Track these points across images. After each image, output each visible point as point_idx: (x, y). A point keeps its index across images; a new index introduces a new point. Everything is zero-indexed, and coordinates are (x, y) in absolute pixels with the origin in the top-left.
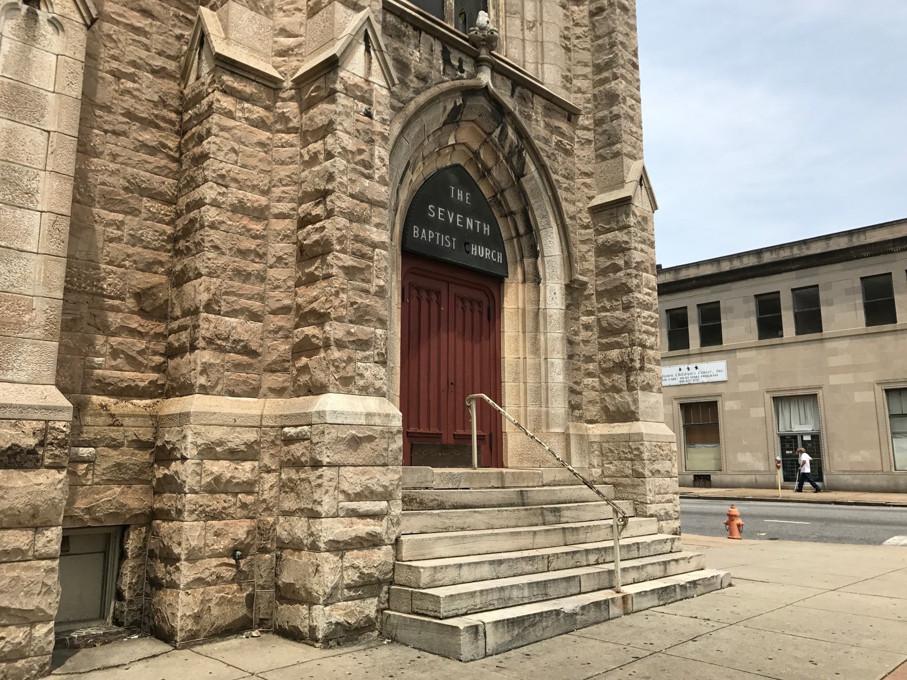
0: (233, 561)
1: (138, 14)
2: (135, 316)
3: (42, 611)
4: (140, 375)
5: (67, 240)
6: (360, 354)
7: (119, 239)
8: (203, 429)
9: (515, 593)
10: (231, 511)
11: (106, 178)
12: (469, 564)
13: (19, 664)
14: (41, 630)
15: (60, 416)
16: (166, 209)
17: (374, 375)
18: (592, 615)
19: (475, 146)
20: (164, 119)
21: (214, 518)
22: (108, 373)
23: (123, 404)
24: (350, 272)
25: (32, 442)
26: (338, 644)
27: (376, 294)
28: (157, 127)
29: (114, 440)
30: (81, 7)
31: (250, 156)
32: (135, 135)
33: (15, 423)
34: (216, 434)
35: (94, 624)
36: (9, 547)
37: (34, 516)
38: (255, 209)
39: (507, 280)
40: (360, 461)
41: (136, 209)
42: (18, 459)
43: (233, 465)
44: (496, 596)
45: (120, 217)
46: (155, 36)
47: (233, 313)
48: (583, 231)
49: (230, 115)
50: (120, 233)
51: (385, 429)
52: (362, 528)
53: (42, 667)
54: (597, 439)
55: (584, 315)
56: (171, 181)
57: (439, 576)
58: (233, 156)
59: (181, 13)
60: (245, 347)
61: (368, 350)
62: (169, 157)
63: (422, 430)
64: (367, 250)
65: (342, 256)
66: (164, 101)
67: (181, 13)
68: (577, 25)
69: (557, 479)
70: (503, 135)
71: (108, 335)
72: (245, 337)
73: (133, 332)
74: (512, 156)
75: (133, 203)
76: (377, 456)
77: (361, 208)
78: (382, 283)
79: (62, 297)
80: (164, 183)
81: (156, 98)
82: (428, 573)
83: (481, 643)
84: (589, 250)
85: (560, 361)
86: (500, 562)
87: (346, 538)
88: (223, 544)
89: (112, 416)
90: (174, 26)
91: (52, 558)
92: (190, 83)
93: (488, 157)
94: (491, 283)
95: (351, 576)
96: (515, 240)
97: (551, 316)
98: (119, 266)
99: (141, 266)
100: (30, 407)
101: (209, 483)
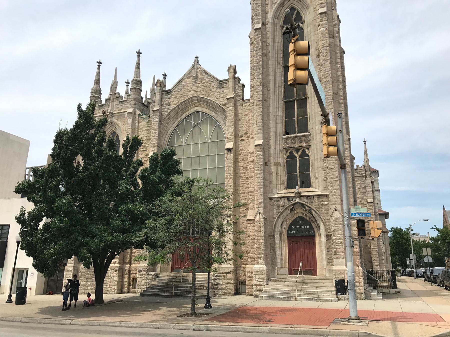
18: (287, 299)
24: (258, 248)
34: (249, 270)
52: (259, 283)
70: (305, 208)
77: (258, 238)
88: (251, 284)
94: (313, 237)
95: (257, 289)
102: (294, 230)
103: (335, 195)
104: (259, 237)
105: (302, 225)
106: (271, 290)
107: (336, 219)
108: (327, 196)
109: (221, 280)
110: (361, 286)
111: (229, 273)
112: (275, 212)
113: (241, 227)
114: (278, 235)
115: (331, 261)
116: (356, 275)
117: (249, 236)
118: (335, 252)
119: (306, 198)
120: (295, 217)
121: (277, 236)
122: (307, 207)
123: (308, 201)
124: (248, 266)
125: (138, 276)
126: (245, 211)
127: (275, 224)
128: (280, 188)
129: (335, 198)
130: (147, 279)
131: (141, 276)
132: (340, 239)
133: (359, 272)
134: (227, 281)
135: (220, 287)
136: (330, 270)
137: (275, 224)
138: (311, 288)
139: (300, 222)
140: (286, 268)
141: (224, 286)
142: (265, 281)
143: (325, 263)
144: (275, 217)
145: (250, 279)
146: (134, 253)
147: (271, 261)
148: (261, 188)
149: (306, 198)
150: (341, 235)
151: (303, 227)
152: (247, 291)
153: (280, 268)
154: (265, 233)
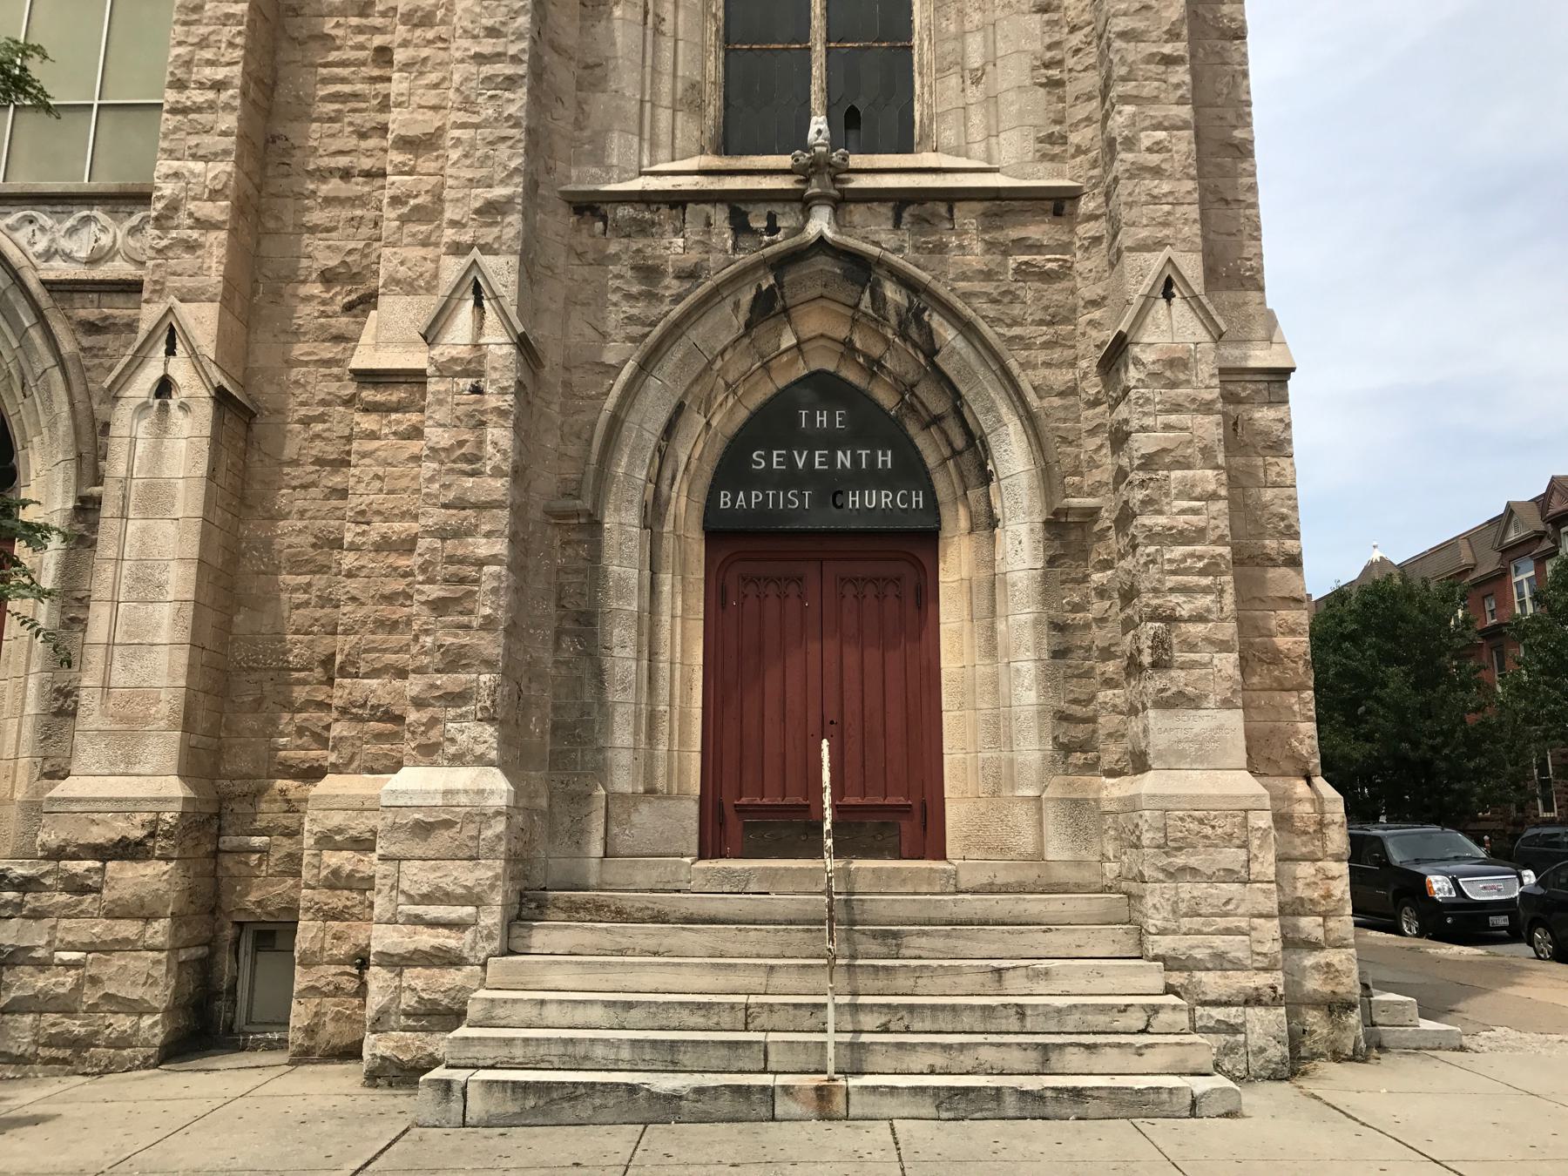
0: (356, 972)
6: (452, 712)
7: (307, 604)
8: (321, 814)
9: (599, 1051)
10: (356, 910)
11: (294, 540)
12: (561, 1002)
14: (147, 1021)
15: (170, 806)
17: (475, 738)
18: (725, 1105)
19: (842, 332)
21: (335, 917)
22: (292, 754)
24: (439, 606)
25: (139, 834)
26: (390, 1085)
27: (481, 628)
31: (400, 477)
33: (128, 814)
34: (337, 819)
37: (142, 907)
38: (404, 541)
39: (942, 534)
40: (431, 853)
43: (358, 856)
44: (556, 1050)
45: (305, 579)
47: (374, 673)
48: (1090, 413)
49: (372, 435)
51: (474, 811)
52: (427, 939)
53: (147, 1058)
54: (1114, 807)
55: (1098, 571)
57: (499, 1012)
58: (377, 484)
60: (386, 712)
61: (465, 704)
63: (766, 801)
64: (470, 571)
65: (426, 587)
68: (1074, 29)
69: (998, 881)
70: (878, 300)
72: (386, 700)
74: (907, 328)
75: (321, 559)
76: (458, 847)
77: (454, 517)
78: (488, 611)
82: (478, 1007)
83: (456, 1106)
84: (1101, 446)
85: (1031, 665)
86: (629, 1006)
87: (401, 951)
88: (343, 950)
89: (288, 801)
91: (161, 950)
93: (870, 342)
94: (918, 544)
95: (408, 1000)
96: (951, 463)
97: (1014, 585)
98: (307, 634)
101: (326, 877)
102: (765, 480)
103: (1157, 172)
104: (460, 504)
105: (832, 441)
106: (552, 1014)
107: (1172, 363)
108: (1059, 204)
109: (37, 915)
110: (1339, 945)
111: (127, 850)
112: (614, 317)
113: (290, 451)
114: (632, 517)
115: (1080, 732)
116: (1300, 846)
117: (362, 517)
118: (1160, 644)
119: (886, 210)
120: (781, 382)
121: (621, 523)
122: (891, 292)
123: (906, 237)
124: (331, 785)
126: (343, 323)
127: (615, 423)
128: (664, 138)
129: (1155, 199)
132: (1199, 535)
133: (1322, 825)
136: (1078, 810)
137: (615, 423)
138: (950, 978)
139: (822, 419)
140: (682, 795)
141: (69, 979)
142: (492, 918)
143: (1031, 749)
144: (610, 357)
145: (339, 900)
147: (554, 738)
148: (511, 82)
149: (886, 210)
150: (1213, 497)
151: (843, 459)
152: (300, 1014)
153: (631, 800)
154: (518, 474)
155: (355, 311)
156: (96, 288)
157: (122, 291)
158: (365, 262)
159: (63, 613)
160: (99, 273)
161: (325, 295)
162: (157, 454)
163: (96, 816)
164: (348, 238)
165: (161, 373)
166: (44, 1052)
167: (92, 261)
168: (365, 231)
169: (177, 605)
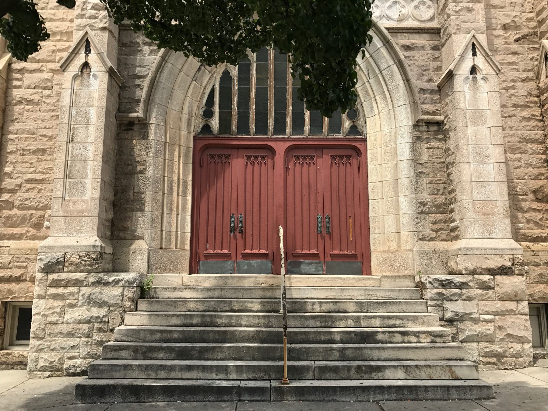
1: (511, 56)
2: (534, 202)
3: (526, 338)
4: (542, 231)
5: (505, 174)
7: (520, 167)
13: (521, 359)
15: (518, 252)
16: (541, 146)
20: (532, 102)
22: (526, 231)
23: (536, 245)
28: (529, 107)
29: (536, 263)
30: (494, 67)
32: (519, 114)
35: (539, 349)
36: (508, 309)
37: (516, 296)
41: (526, 150)
42: (505, 271)
45: (519, 156)
46: (521, 63)
50: (520, 163)
56: (541, 132)
59: (531, 46)
62: (537, 120)
66: (530, 94)
67: (531, 46)
71: (523, 213)
73: (535, 210)
75: (524, 148)
79: (508, 199)
80: (537, 134)
81: (526, 93)
89: (533, 251)
90: (528, 54)
91: (527, 315)
92: (542, 80)
98: (523, 179)
99: (533, 177)
100: (506, 249)
109: (469, 299)
111: (504, 271)
125: (37, 290)
130: (91, 301)
131: (60, 291)
134: (499, 305)
135: (469, 329)
141: (491, 326)
146: (13, 191)
155: (520, 42)
156: (407, 31)
157: (418, 33)
158: (521, 21)
159: (416, 170)
160: (405, 24)
161: (505, 35)
162: (475, 99)
163: (487, 256)
164: (511, 11)
165: (472, 64)
166: (485, 360)
167: (400, 20)
168: (518, 8)
169: (498, 164)
